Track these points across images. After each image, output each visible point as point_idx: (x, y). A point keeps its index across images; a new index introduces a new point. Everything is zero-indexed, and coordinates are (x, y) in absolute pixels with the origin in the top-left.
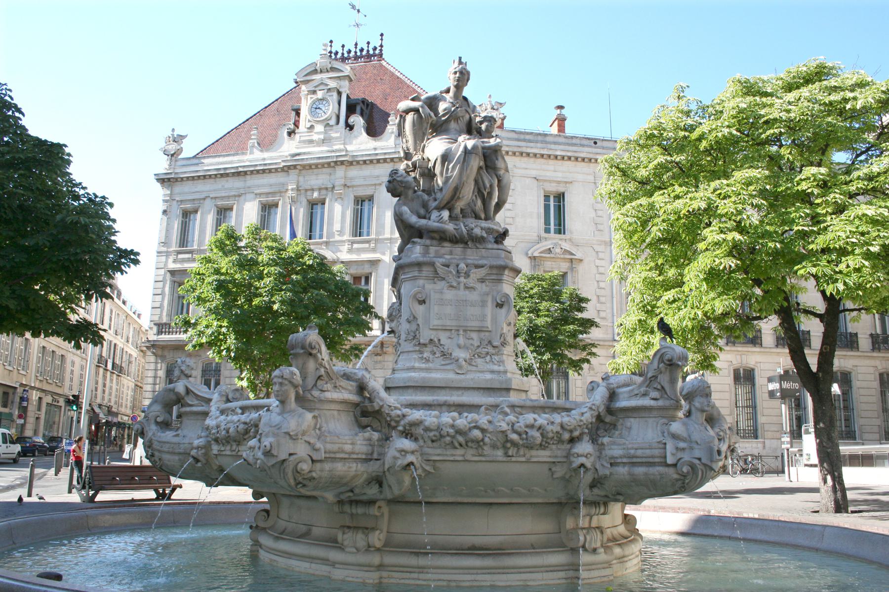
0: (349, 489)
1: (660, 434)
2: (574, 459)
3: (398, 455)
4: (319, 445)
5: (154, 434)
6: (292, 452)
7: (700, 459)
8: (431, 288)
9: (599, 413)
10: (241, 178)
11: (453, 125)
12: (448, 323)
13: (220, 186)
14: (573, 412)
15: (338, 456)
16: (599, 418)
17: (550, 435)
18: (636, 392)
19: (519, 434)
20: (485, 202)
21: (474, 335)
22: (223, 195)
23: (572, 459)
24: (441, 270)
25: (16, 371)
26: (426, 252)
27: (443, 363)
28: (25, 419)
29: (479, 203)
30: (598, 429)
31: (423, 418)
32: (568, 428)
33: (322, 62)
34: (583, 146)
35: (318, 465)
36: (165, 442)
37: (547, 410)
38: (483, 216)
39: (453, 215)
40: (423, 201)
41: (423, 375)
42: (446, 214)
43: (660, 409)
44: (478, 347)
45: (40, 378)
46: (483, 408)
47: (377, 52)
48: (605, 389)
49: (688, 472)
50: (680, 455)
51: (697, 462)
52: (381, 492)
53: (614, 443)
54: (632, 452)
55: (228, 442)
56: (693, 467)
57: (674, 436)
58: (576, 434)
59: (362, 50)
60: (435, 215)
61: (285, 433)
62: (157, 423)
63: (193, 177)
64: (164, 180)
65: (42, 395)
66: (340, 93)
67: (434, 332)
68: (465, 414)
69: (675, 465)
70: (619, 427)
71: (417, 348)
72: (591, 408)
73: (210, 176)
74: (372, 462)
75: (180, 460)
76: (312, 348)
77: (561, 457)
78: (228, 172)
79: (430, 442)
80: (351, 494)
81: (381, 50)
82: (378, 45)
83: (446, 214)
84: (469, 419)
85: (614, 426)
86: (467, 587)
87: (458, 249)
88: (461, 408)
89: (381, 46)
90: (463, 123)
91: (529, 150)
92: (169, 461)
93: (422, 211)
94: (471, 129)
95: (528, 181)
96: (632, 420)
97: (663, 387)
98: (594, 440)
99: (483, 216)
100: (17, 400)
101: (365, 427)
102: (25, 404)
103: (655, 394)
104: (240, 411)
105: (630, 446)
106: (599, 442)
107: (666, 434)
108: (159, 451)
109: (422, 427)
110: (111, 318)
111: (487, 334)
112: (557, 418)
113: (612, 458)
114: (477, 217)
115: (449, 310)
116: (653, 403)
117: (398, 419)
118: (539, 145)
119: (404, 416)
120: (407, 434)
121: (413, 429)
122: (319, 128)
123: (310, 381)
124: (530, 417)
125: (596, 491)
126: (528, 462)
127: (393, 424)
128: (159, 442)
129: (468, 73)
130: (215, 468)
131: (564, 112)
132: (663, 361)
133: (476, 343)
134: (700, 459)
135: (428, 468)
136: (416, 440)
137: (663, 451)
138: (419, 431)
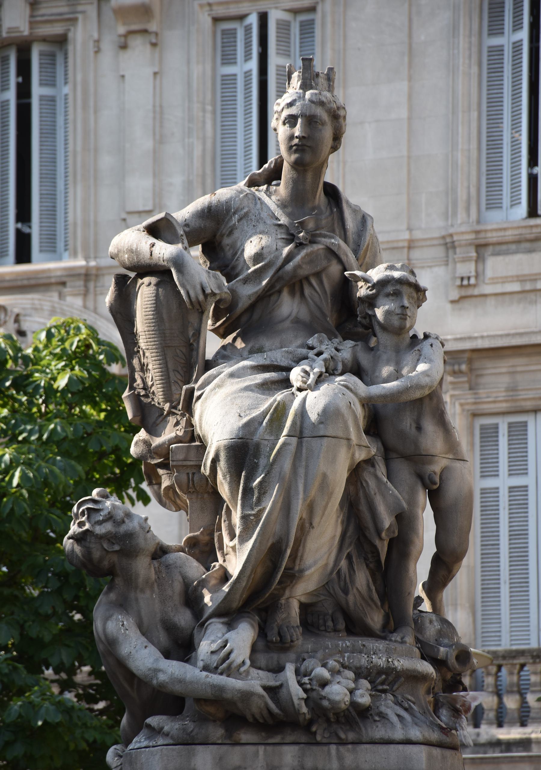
11: (287, 306)
20: (389, 572)
29: (362, 578)
38: (375, 619)
40: (186, 584)
42: (242, 639)
86: (55, 515)
90: (319, 294)
99: (375, 619)
114: (355, 627)
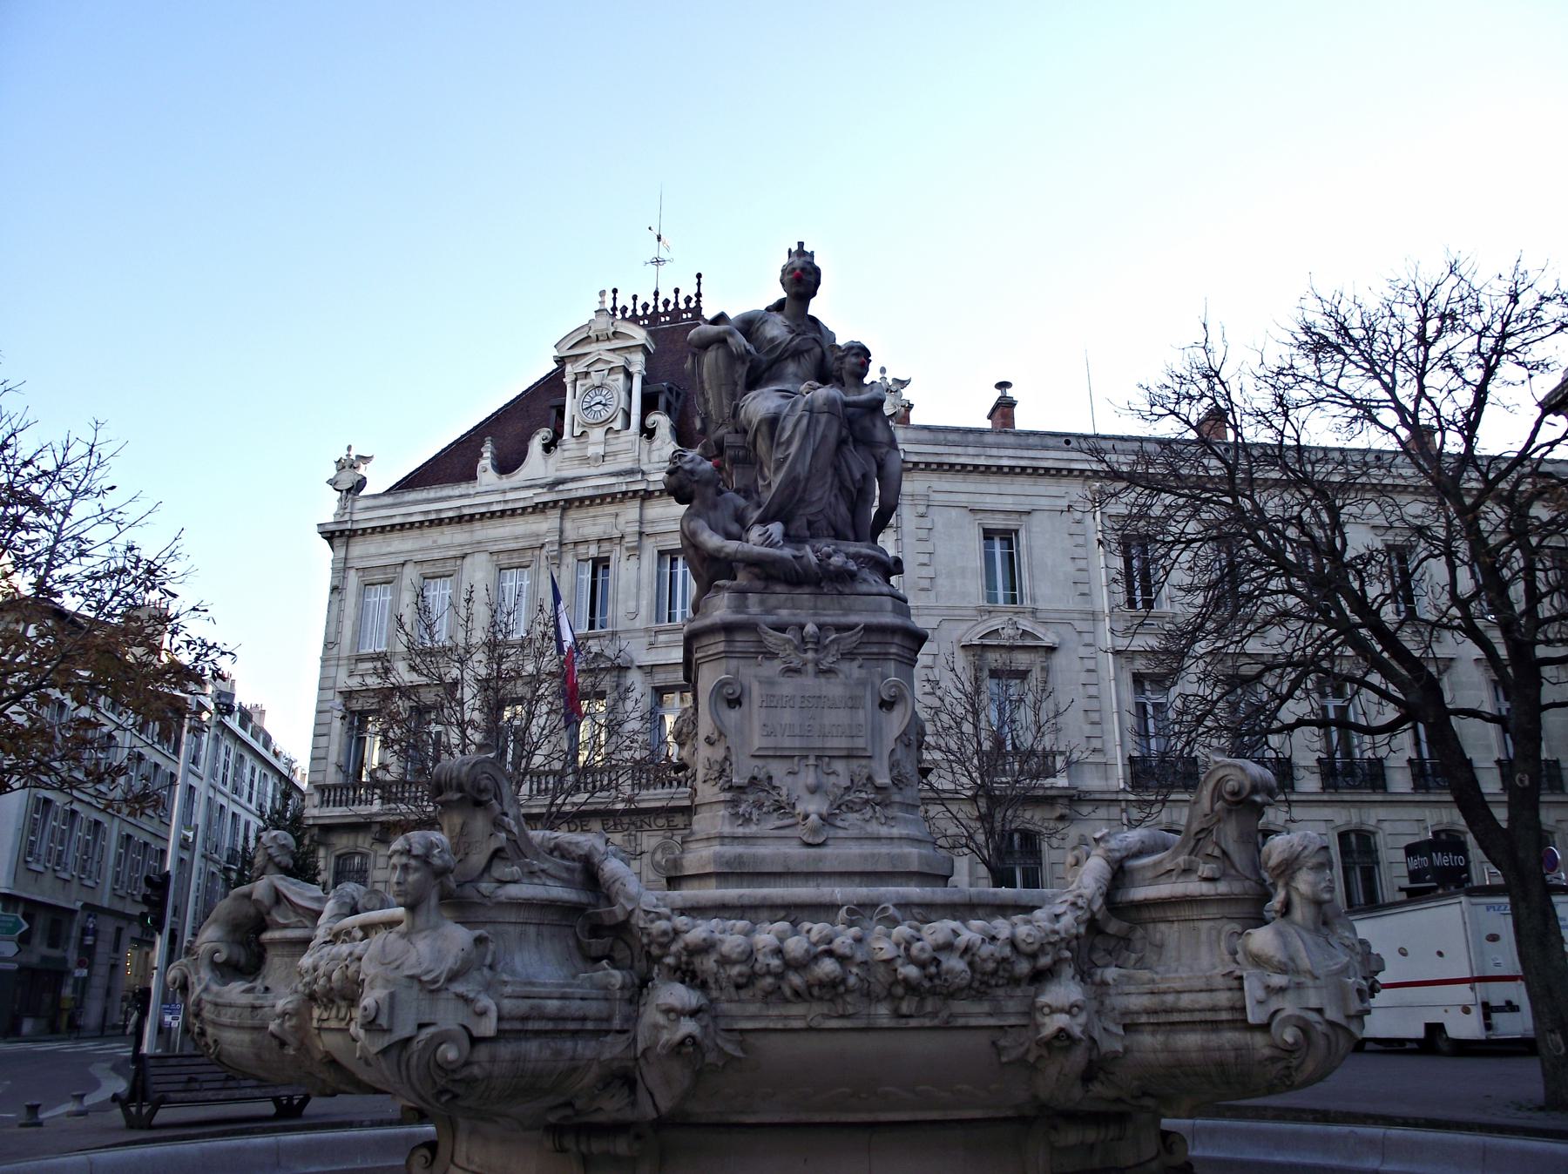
0: (561, 1100)
1: (1227, 957)
2: (1047, 1020)
3: (661, 1019)
4: (485, 1001)
5: (206, 989)
6: (426, 1020)
7: (1320, 1011)
8: (753, 675)
9: (1093, 914)
10: (467, 527)
12: (787, 743)
13: (430, 543)
14: (1038, 913)
15: (531, 1026)
16: (1093, 926)
17: (991, 966)
18: (1169, 867)
19: (922, 965)
21: (839, 766)
22: (436, 556)
23: (1039, 1018)
24: (773, 638)
25: (76, 880)
26: (740, 607)
27: (779, 823)
28: (90, 967)
30: (1092, 949)
31: (717, 936)
32: (1029, 949)
33: (603, 324)
34: (1046, 448)
35: (483, 1052)
36: (225, 1005)
37: (980, 912)
39: (792, 533)
41: (739, 849)
43: (1222, 900)
44: (847, 789)
45: (120, 892)
46: (842, 913)
47: (692, 305)
48: (1103, 863)
49: (1296, 1043)
50: (1274, 1004)
51: (1313, 1017)
52: (634, 1104)
53: (1129, 979)
54: (1170, 999)
55: (332, 1001)
56: (1304, 1028)
57: (1258, 961)
58: (1044, 961)
59: (666, 303)
60: (755, 533)
61: (411, 977)
62: (215, 966)
63: (383, 527)
64: (330, 536)
65: (123, 924)
66: (629, 376)
67: (759, 762)
68: (807, 925)
69: (1265, 1028)
70: (1138, 945)
71: (728, 796)
72: (1074, 904)
73: (412, 524)
74: (609, 1038)
75: (253, 1042)
76: (481, 791)
77: (1016, 1014)
78: (443, 515)
79: (732, 990)
80: (569, 1112)
81: (698, 302)
82: (692, 292)
83: (776, 529)
84: (814, 936)
85: (1125, 941)
87: (804, 597)
88: (795, 912)
89: (699, 295)
90: (808, 363)
91: (953, 460)
92: (231, 1044)
93: (734, 528)
94: (824, 376)
95: (954, 512)
96: (1162, 927)
97: (1224, 852)
98: (1084, 975)
100: (75, 932)
101: (598, 960)
102: (89, 940)
103: (1205, 869)
104: (359, 934)
105: (1163, 986)
106: (1097, 978)
107: (1240, 957)
108: (215, 1024)
109: (713, 957)
110: (252, 782)
111: (864, 762)
112: (1002, 927)
113: (1126, 1013)
115: (787, 716)
116: (1205, 889)
117: (664, 940)
118: (971, 450)
119: (677, 933)
120: (687, 974)
121: (697, 960)
122: (597, 434)
123: (478, 859)
124: (941, 928)
125: (1096, 1088)
126: (946, 1027)
127: (655, 951)
128: (216, 1005)
129: (817, 271)
130: (318, 1056)
131: (1009, 392)
132: (1221, 797)
133: (845, 782)
134: (1320, 1011)
135: (730, 1048)
136: (703, 986)
137: (1237, 994)
138: (709, 963)
